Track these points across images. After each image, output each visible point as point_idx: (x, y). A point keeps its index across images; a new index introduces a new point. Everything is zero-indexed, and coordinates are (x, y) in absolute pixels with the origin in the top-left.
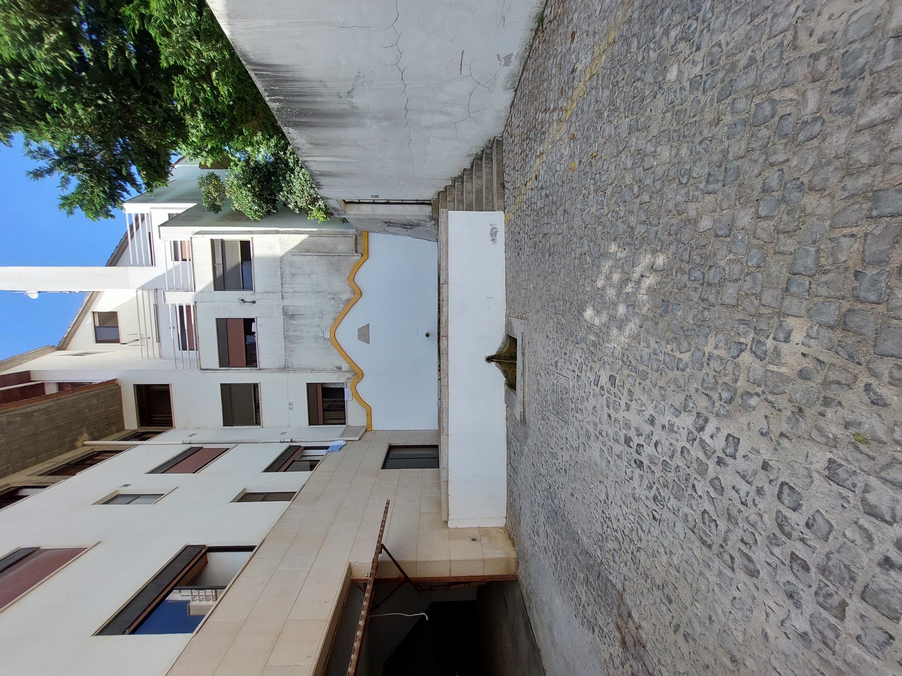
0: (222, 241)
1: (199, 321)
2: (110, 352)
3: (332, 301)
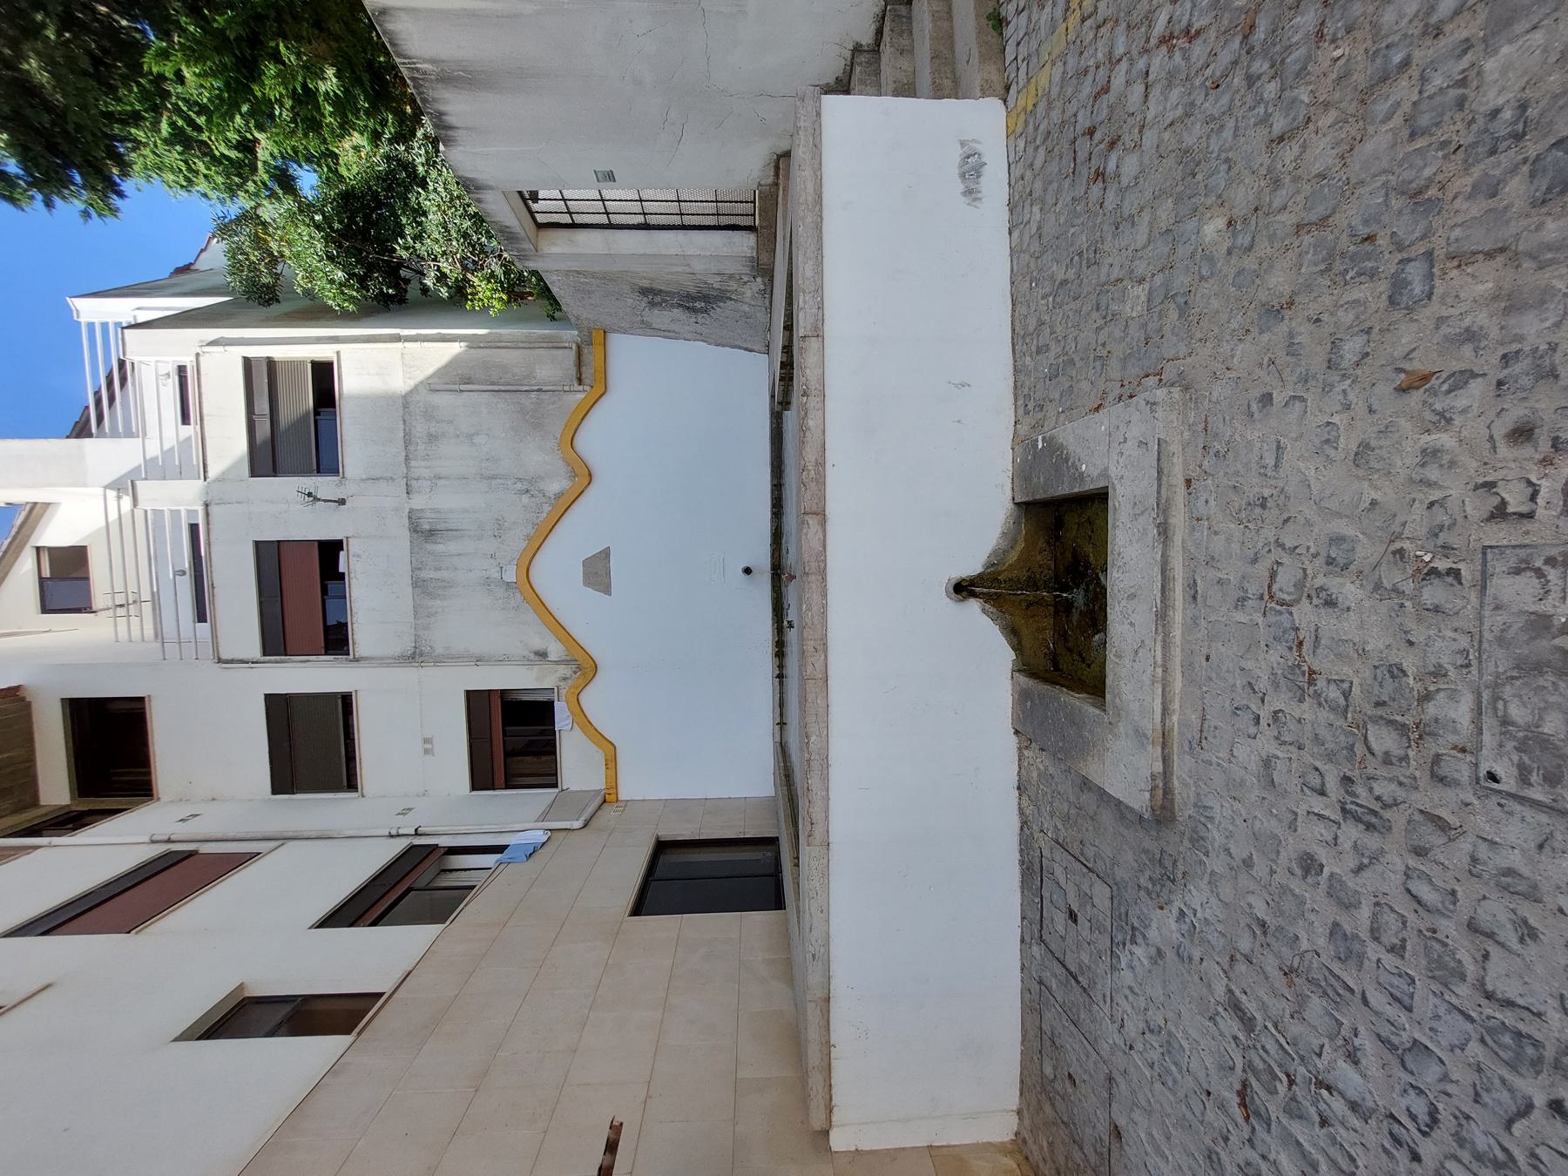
0: (271, 363)
1: (214, 549)
2: (69, 631)
3: (525, 499)
